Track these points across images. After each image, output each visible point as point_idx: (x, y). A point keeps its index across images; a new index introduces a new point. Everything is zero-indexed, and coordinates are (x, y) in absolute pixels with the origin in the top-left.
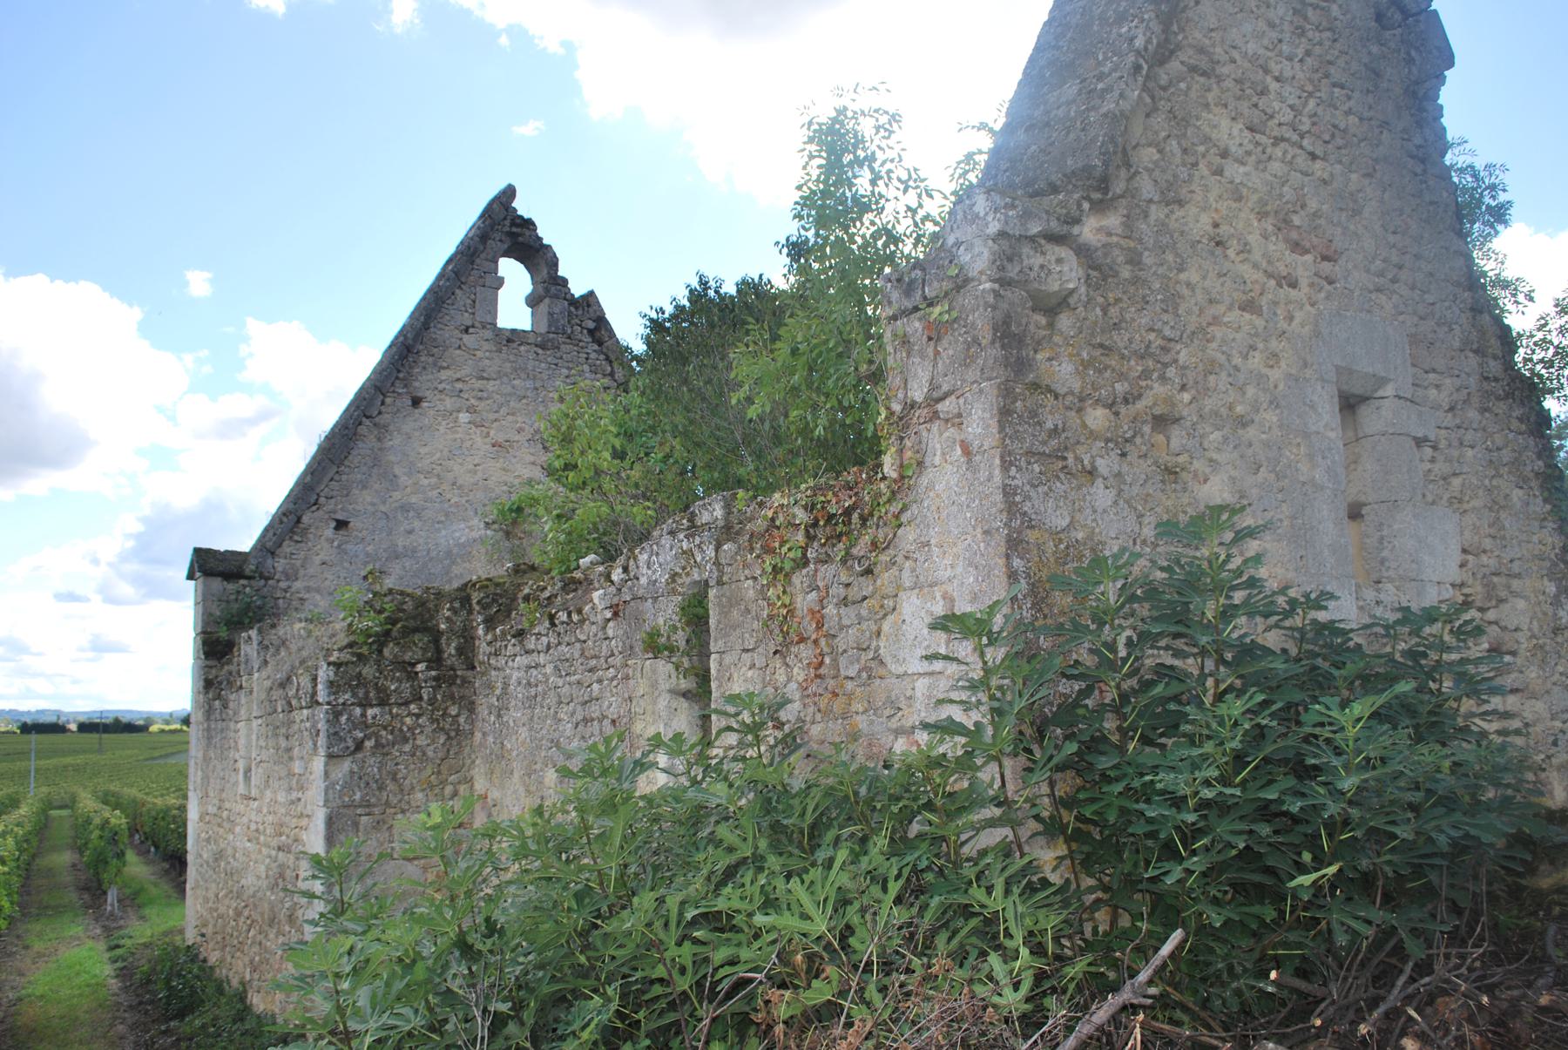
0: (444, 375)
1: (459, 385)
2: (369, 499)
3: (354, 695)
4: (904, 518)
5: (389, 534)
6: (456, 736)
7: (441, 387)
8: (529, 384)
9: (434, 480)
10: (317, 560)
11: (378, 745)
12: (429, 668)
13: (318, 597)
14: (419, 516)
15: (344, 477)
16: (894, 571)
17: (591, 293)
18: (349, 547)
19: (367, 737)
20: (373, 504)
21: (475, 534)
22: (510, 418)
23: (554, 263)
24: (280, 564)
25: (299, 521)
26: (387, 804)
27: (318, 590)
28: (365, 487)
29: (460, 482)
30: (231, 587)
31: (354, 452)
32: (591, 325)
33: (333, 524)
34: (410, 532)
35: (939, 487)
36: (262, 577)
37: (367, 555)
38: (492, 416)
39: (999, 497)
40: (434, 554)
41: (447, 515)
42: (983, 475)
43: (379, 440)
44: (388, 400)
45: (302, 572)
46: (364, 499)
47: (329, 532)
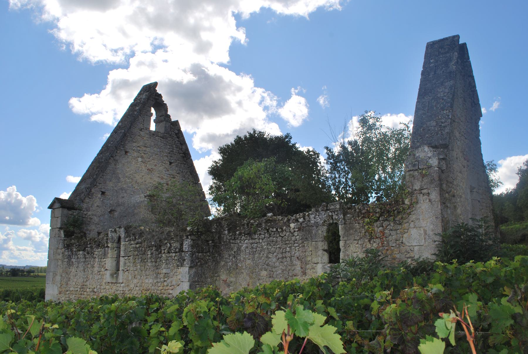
0: (135, 144)
1: (139, 148)
2: (111, 185)
3: (197, 249)
4: (412, 213)
5: (117, 197)
6: (217, 263)
7: (134, 148)
8: (158, 150)
9: (130, 180)
10: (96, 205)
11: (201, 264)
12: (212, 243)
13: (95, 218)
14: (126, 192)
15: (104, 177)
16: (408, 224)
17: (177, 121)
18: (105, 201)
19: (199, 262)
20: (113, 187)
21: (142, 200)
22: (153, 161)
23: (166, 110)
24: (85, 206)
25: (90, 191)
26: (202, 282)
27: (95, 215)
28: (111, 181)
29: (138, 181)
30: (70, 212)
31: (108, 169)
32: (177, 132)
33: (101, 193)
34: (123, 197)
35: (423, 208)
36: (79, 210)
37: (110, 204)
38: (148, 160)
39: (440, 211)
40: (130, 205)
41: (134, 192)
42: (435, 206)
43: (115, 165)
44: (118, 152)
45: (91, 209)
46: (110, 185)
47: (99, 196)
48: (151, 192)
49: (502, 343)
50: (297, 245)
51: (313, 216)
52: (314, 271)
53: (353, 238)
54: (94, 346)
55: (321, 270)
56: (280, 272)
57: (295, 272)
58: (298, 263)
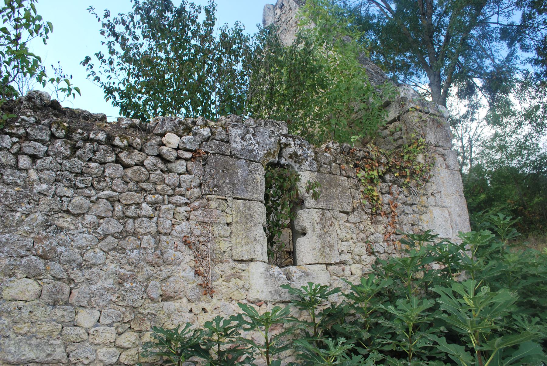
48: (44, 198)
49: (449, 355)
50: (184, 200)
51: (239, 131)
52: (240, 283)
53: (339, 208)
54: (119, 40)
55: (262, 281)
56: (109, 283)
57: (170, 287)
58: (187, 257)
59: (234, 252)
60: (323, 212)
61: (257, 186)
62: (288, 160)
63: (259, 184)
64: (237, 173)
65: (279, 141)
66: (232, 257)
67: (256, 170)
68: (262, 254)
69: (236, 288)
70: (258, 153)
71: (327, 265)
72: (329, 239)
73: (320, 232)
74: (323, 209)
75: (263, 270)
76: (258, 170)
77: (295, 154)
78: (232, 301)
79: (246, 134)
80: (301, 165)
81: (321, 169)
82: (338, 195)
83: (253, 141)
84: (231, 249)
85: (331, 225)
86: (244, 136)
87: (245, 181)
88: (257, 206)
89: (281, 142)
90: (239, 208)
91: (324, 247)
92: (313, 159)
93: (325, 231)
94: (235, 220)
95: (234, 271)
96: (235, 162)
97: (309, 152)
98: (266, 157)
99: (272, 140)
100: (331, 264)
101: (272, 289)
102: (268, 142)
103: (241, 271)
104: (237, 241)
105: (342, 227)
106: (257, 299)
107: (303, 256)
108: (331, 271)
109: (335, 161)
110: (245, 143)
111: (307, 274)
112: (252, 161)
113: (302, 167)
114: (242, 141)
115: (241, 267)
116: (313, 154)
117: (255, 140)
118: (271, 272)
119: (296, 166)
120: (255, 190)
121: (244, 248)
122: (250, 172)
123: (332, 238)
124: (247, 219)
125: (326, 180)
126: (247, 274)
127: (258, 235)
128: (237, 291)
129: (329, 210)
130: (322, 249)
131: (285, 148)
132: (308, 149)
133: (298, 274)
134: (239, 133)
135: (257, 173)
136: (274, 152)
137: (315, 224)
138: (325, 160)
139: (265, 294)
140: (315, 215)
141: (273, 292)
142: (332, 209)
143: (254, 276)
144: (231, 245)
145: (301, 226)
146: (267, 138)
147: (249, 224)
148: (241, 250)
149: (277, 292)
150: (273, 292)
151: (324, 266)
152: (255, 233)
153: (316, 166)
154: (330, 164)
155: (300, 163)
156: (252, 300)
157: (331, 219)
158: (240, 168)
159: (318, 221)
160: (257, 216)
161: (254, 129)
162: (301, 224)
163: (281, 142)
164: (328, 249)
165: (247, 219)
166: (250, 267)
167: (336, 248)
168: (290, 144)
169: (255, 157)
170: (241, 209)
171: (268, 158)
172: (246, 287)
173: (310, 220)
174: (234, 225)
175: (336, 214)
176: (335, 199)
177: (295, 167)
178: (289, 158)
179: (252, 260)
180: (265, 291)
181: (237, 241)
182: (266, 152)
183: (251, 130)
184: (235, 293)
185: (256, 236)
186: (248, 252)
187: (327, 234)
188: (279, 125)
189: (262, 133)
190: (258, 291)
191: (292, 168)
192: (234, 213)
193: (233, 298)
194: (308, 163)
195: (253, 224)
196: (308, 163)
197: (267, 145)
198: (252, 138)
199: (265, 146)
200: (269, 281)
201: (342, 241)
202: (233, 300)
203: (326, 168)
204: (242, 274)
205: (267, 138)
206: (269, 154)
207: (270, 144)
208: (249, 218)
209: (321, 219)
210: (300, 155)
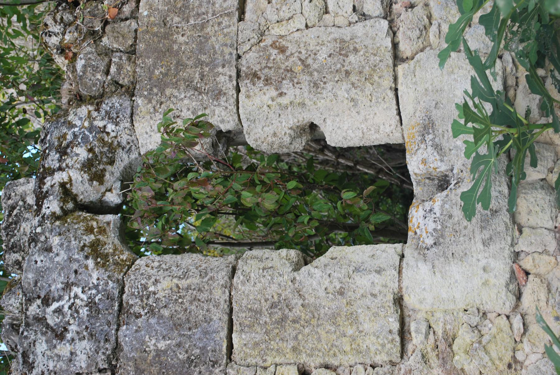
51: (41, 347)
52: (465, 337)
55: (455, 270)
59: (379, 359)
60: (247, 76)
61: (188, 288)
62: (108, 185)
63: (183, 283)
64: (159, 354)
65: (58, 218)
66: (393, 364)
67: (145, 294)
68: (379, 272)
69: (482, 354)
70: (96, 287)
71: (397, 58)
72: (322, 56)
73: (305, 86)
74: (238, 76)
75: (424, 269)
76: (145, 287)
77: (87, 166)
78: (516, 361)
79: (48, 326)
80: (119, 145)
81: (124, 81)
82: (194, 26)
83: (65, 303)
84: (373, 367)
85: (282, 50)
86: (53, 330)
87: (177, 326)
88: (247, 288)
89: (58, 211)
90: (257, 344)
91: (348, 73)
92: (98, 110)
93: (299, 68)
94: (291, 357)
95: (432, 355)
96: (129, 359)
97: (78, 123)
98: (105, 257)
99: (55, 241)
100: (395, 45)
101: (478, 237)
102: (63, 255)
103: (431, 336)
104: (347, 348)
105: (285, 13)
106: (507, 285)
107: (378, 131)
108: (415, 47)
109: (94, 36)
110: (73, 328)
111: (428, 127)
112: (121, 305)
113: (124, 143)
114: (69, 336)
115: (421, 337)
116: (84, 110)
117: (60, 298)
118: (430, 241)
119: (123, 160)
120: (203, 296)
121: (366, 326)
122: (152, 312)
123: (318, 43)
124: (284, 319)
125: (155, 66)
126: (439, 315)
127: (327, 283)
128: (489, 347)
129: (239, 57)
130: (354, 78)
131: (74, 198)
132: (71, 125)
133: (429, 153)
134: (44, 346)
135: (152, 289)
136: (90, 230)
137: (284, 101)
138: (95, 69)
139: (493, 263)
140: (257, 101)
141: (486, 234)
142: (236, 46)
143: (444, 295)
144: (360, 368)
145: (293, 139)
146: (51, 259)
147: (297, 311)
148: (373, 338)
149: (484, 225)
150: (486, 234)
151: (401, 69)
152: (322, 293)
153: (115, 101)
154: (108, 53)
155: (112, 148)
156: (512, 298)
157: (265, 49)
158: (143, 343)
159: (274, 93)
160: (274, 287)
161: (30, 301)
162: (287, 139)
163: (58, 211)
164: (352, 58)
165: (284, 319)
166: (417, 306)
167: (346, 33)
168: (63, 185)
169: (109, 297)
170: (258, 338)
171: (109, 249)
172: (475, 320)
173: (271, 115)
174: (303, 359)
175: (248, 33)
176: (207, 38)
177: (126, 162)
178: (101, 182)
179: (399, 301)
180: (483, 262)
181: (347, 348)
182: (90, 263)
183: (34, 309)
184: (494, 355)
185: (330, 289)
186: (376, 315)
187: (310, 61)
188: (13, 208)
189: (41, 273)
190: (485, 283)
191: (130, 167)
192: (270, 360)
193: (508, 358)
194: (110, 127)
195: (296, 301)
196: (110, 127)
197: (70, 260)
198: (55, 305)
199: (75, 266)
200: (453, 248)
201: (327, 12)
202: (514, 357)
203: (120, 68)
204: (440, 332)
205: (51, 259)
206: (95, 250)
207: (69, 249)
208: (280, 314)
209: (268, 81)
210: (90, 150)
